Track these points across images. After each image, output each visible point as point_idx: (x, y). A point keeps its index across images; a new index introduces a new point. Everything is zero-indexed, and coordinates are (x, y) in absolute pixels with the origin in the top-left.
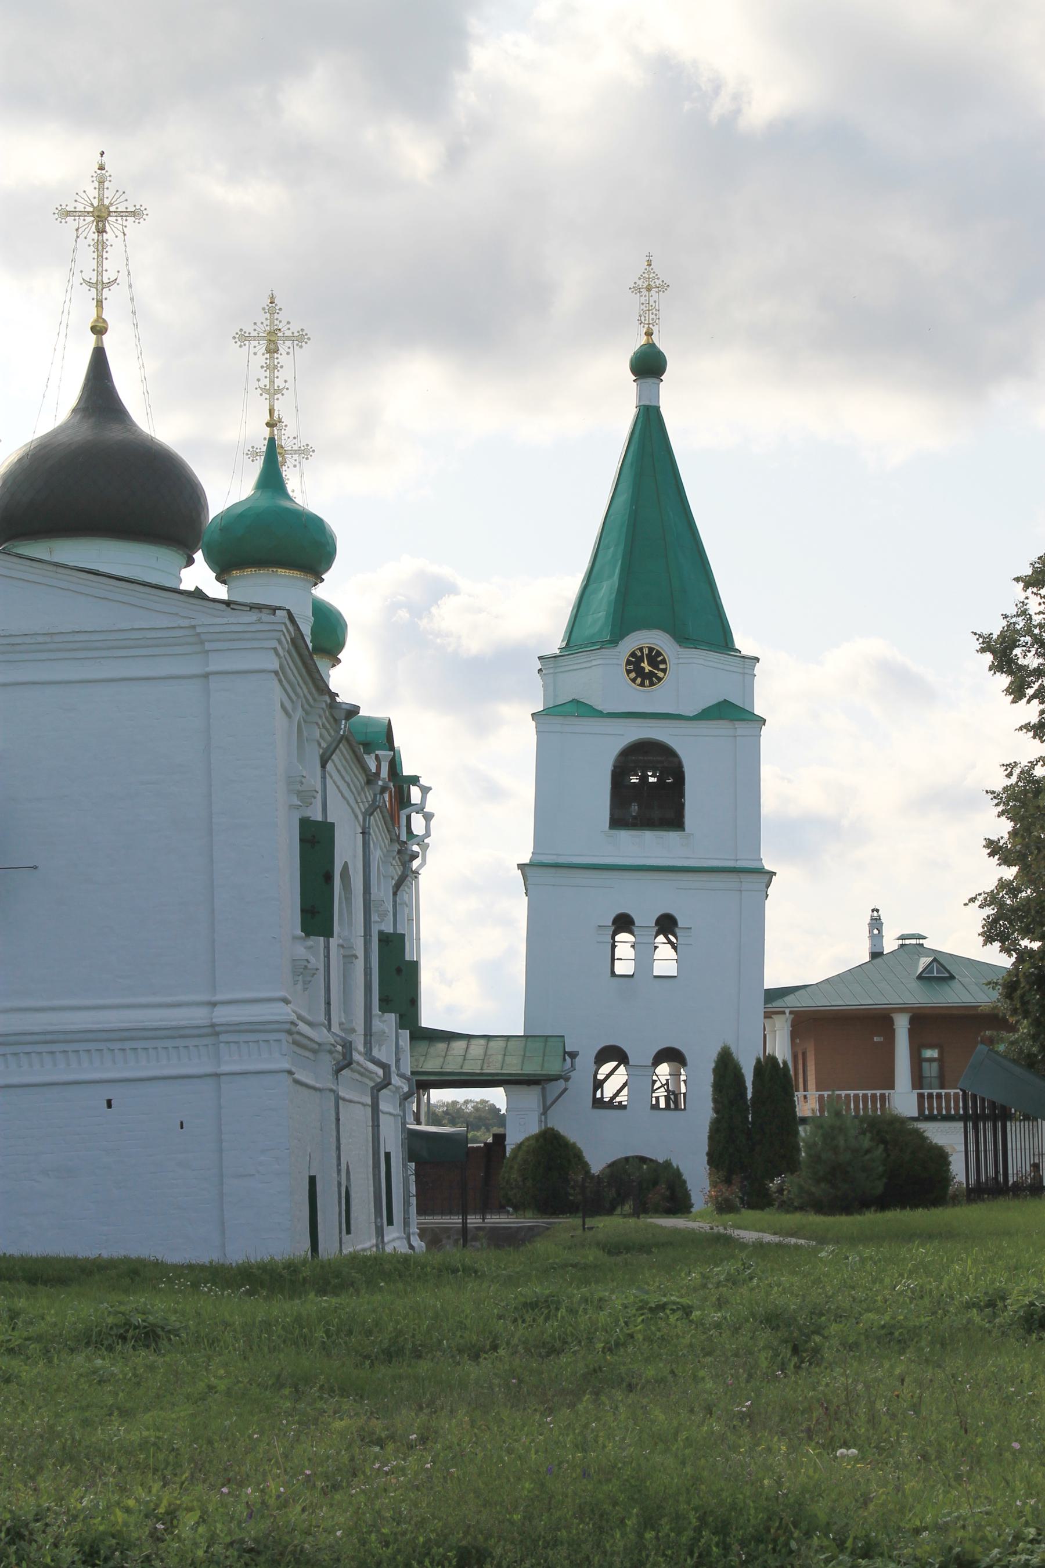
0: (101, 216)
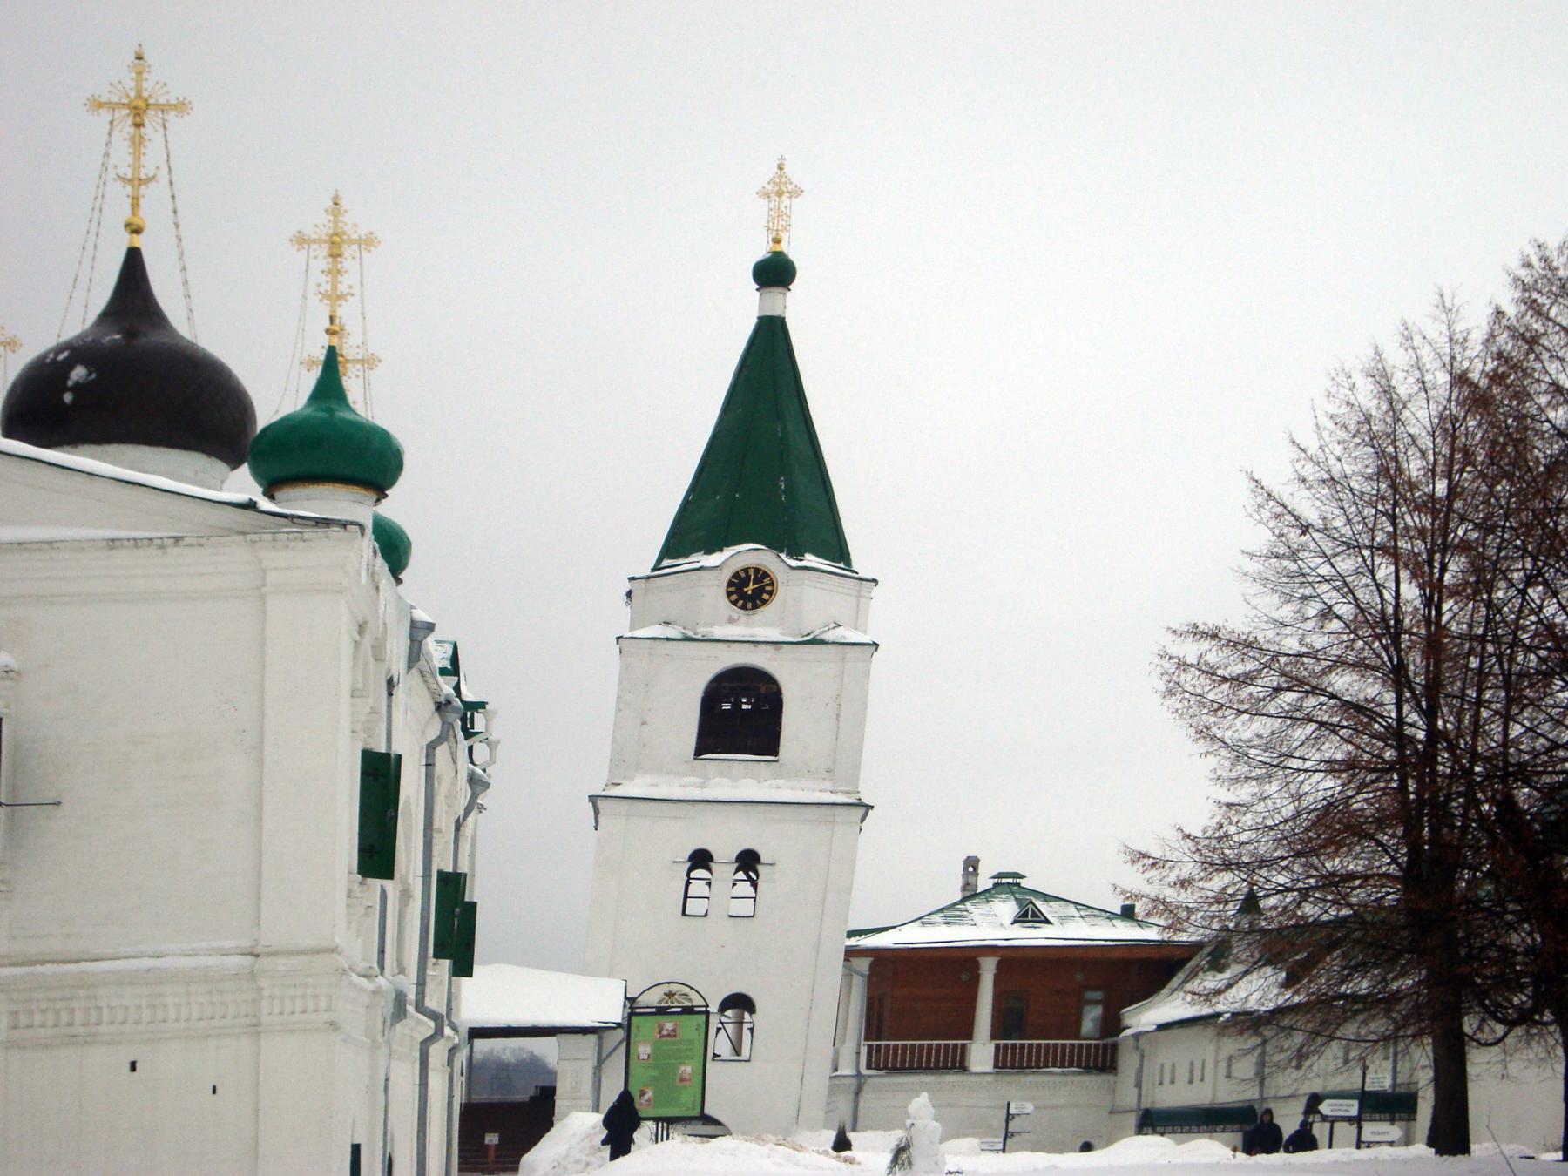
0: (138, 111)
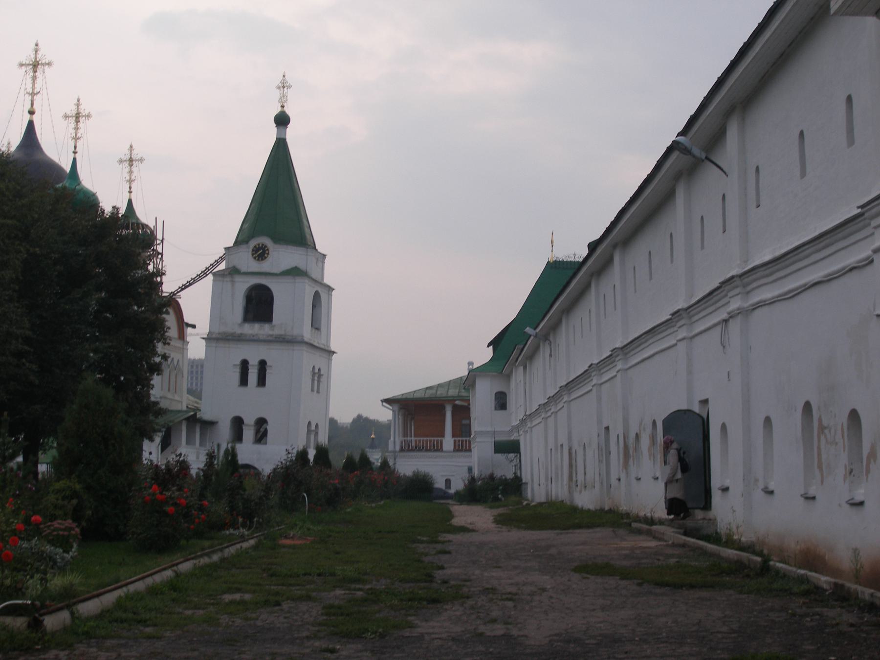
0: (35, 65)
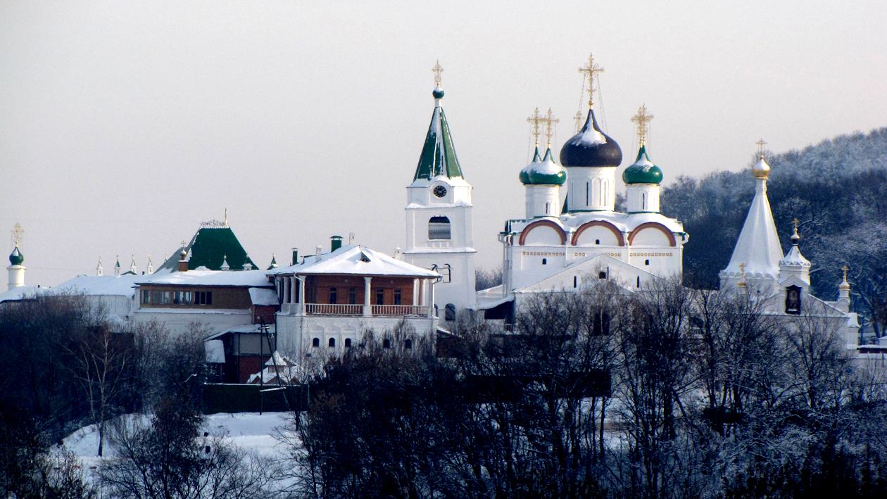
0: (591, 71)
